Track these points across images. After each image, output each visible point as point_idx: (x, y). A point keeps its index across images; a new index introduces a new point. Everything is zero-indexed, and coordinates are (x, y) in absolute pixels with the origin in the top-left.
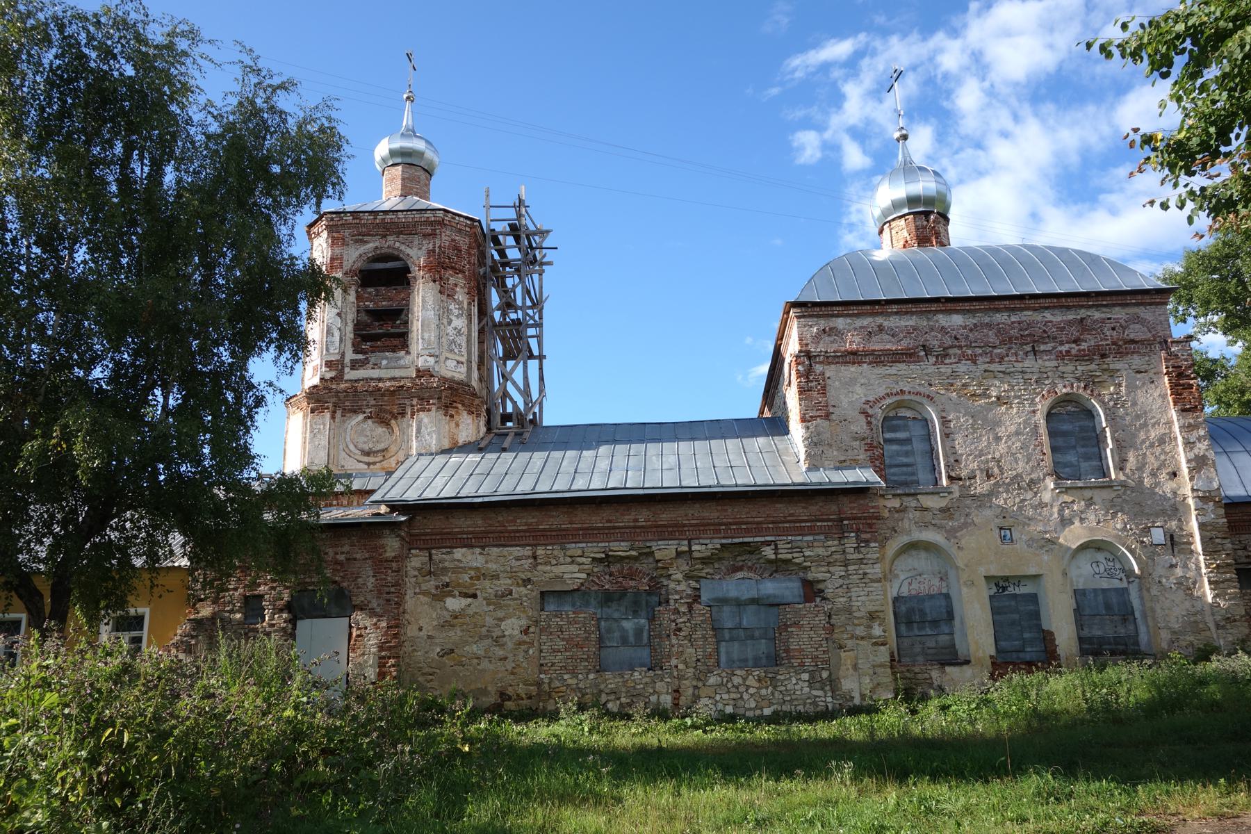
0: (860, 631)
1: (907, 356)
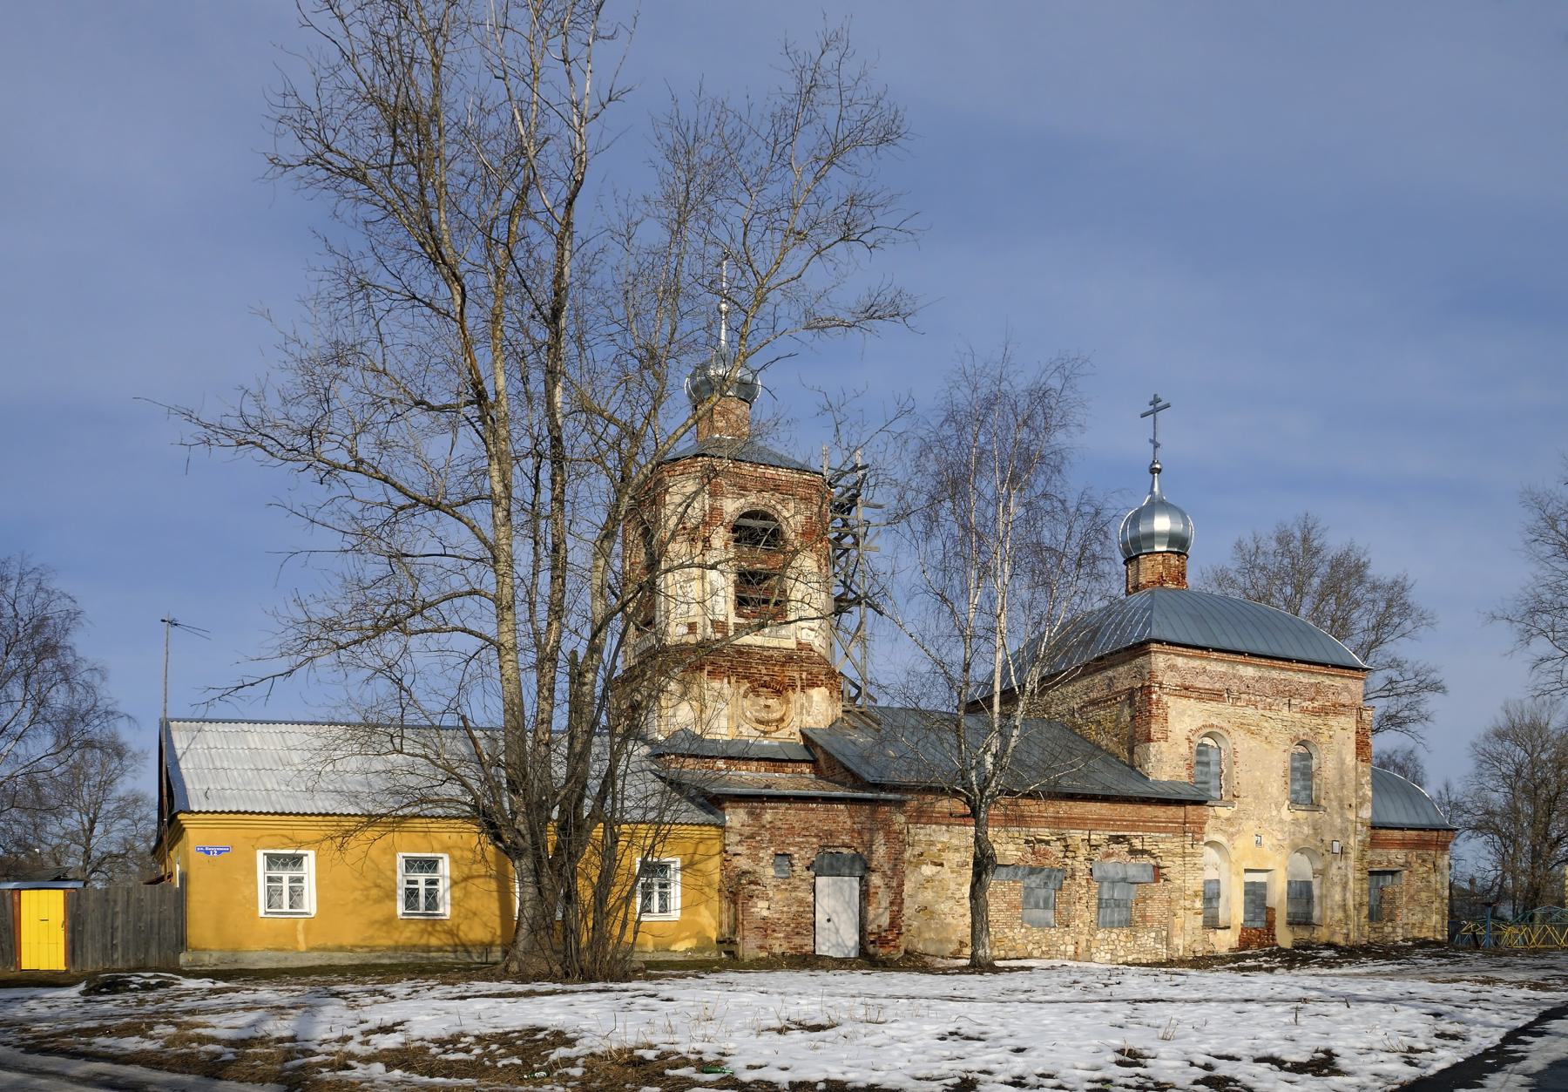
0: (1188, 904)
1: (1216, 696)
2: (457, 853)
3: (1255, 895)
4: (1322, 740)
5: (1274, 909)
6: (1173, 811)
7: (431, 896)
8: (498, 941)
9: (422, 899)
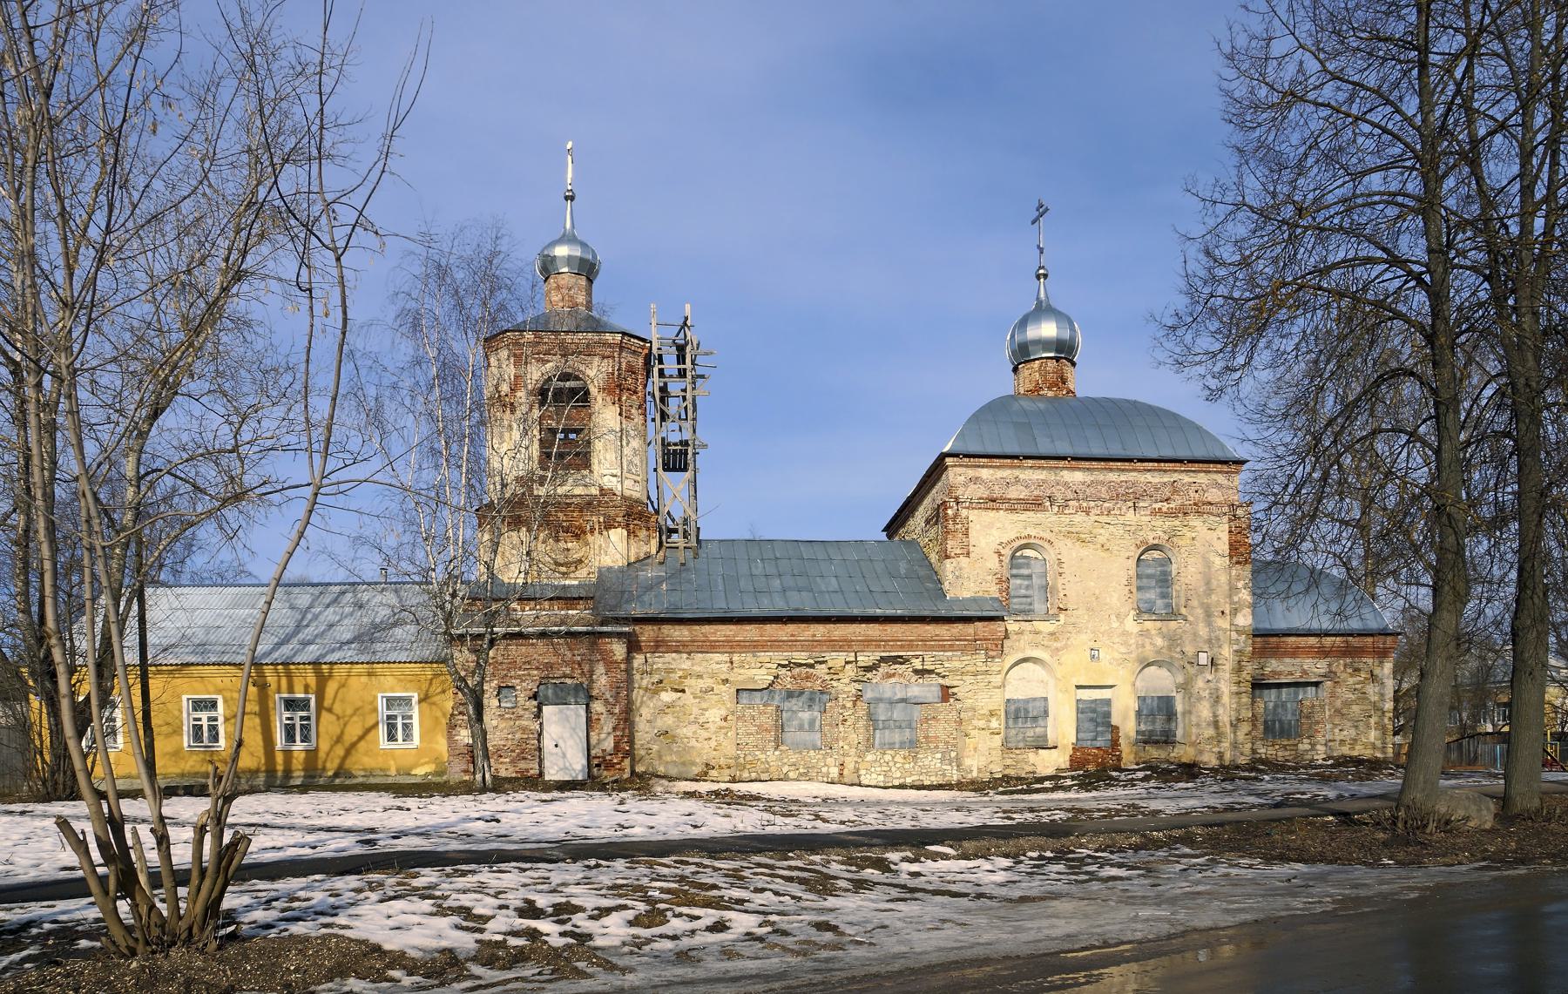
0: (982, 724)
1: (1035, 504)
2: (228, 695)
3: (1095, 716)
4: (1181, 543)
5: (1118, 728)
6: (958, 628)
7: (213, 729)
8: (263, 768)
9: (206, 734)
